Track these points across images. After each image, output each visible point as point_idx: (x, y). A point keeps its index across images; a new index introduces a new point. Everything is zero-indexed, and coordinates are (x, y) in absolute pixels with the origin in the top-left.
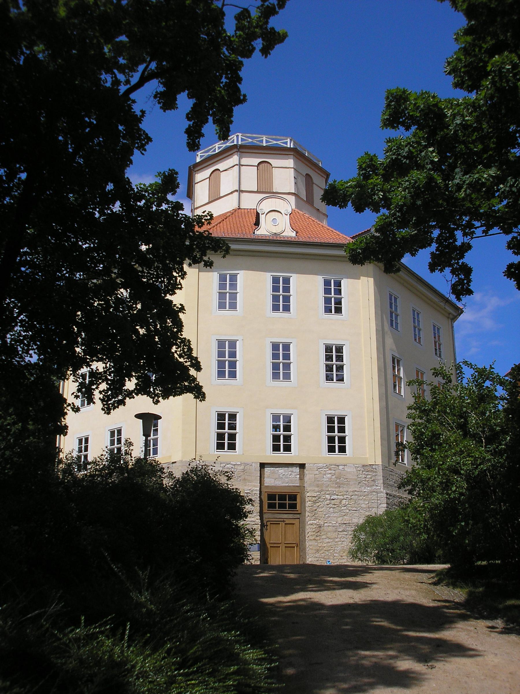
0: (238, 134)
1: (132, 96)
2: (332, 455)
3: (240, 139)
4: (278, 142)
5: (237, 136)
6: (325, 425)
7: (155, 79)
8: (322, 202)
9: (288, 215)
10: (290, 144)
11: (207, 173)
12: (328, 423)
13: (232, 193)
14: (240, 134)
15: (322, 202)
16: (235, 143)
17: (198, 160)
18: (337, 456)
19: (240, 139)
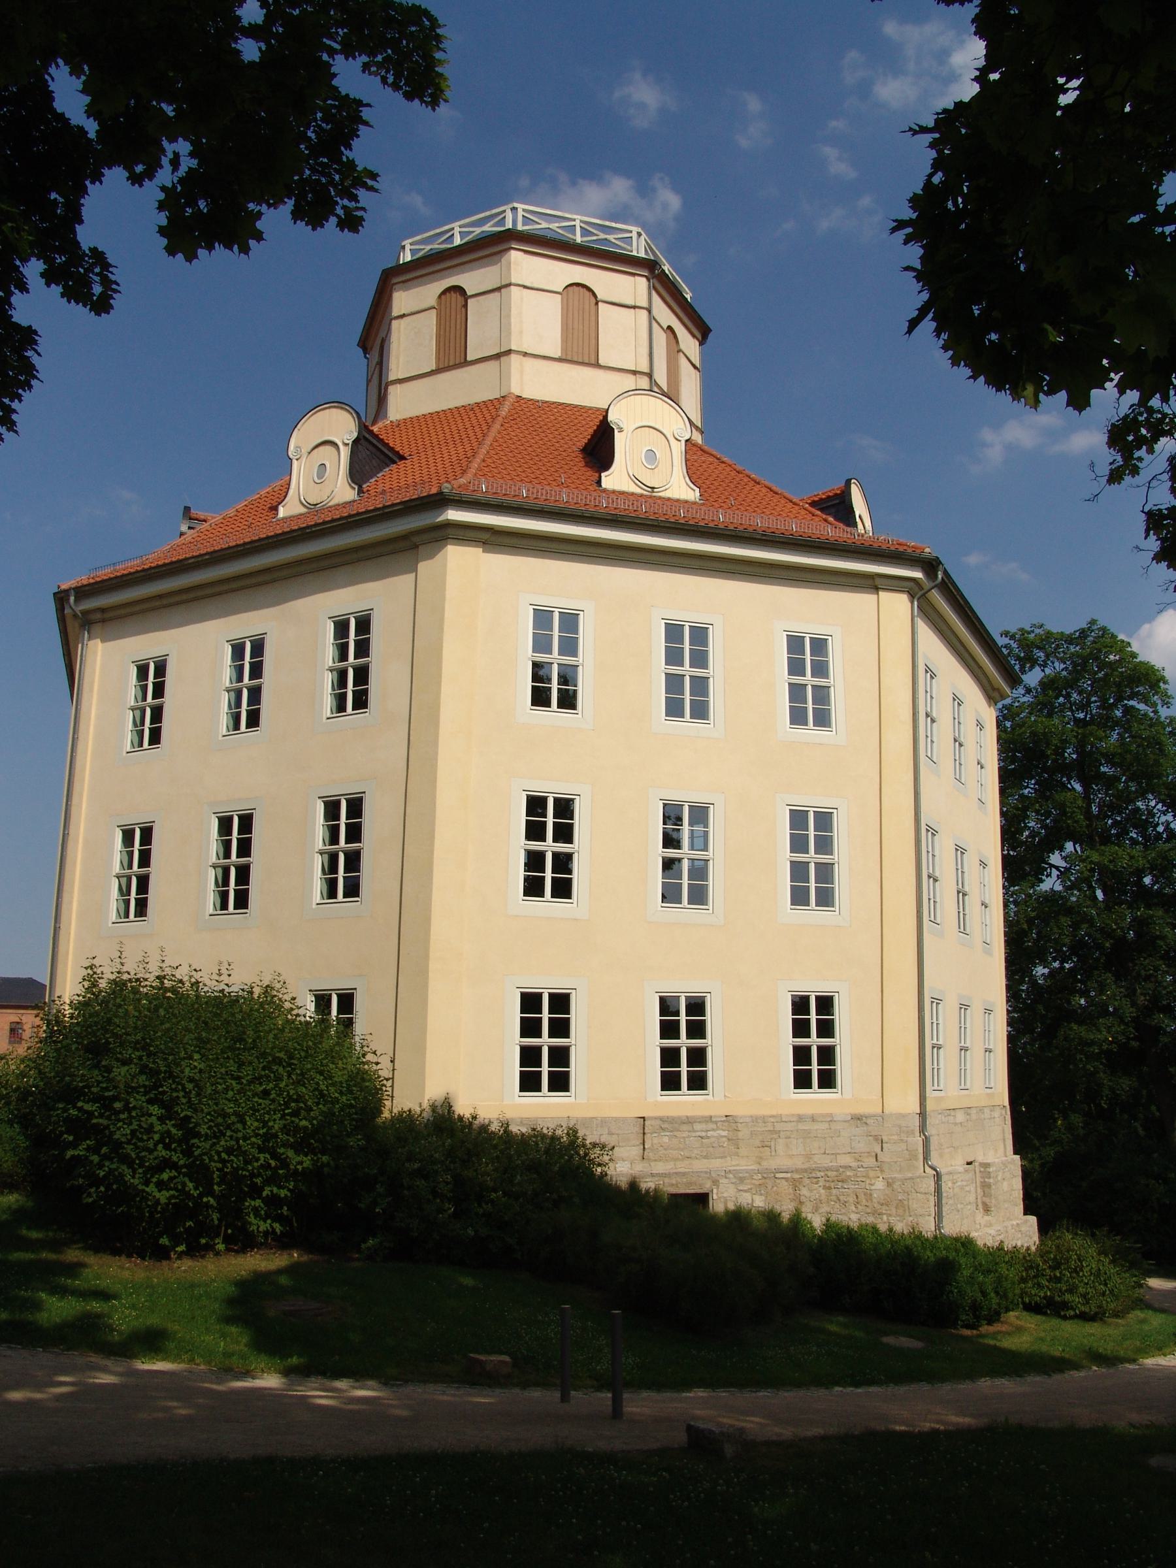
0: (516, 205)
1: (931, 124)
2: (804, 1095)
3: (520, 218)
4: (554, 226)
5: (514, 209)
6: (787, 1018)
7: (984, 52)
8: (259, 236)
9: (683, 443)
10: (639, 249)
11: (427, 293)
12: (571, 826)
13: (403, 316)
14: (520, 206)
15: (259, 236)
16: (509, 225)
17: (407, 257)
18: (815, 1096)
19: (520, 218)
